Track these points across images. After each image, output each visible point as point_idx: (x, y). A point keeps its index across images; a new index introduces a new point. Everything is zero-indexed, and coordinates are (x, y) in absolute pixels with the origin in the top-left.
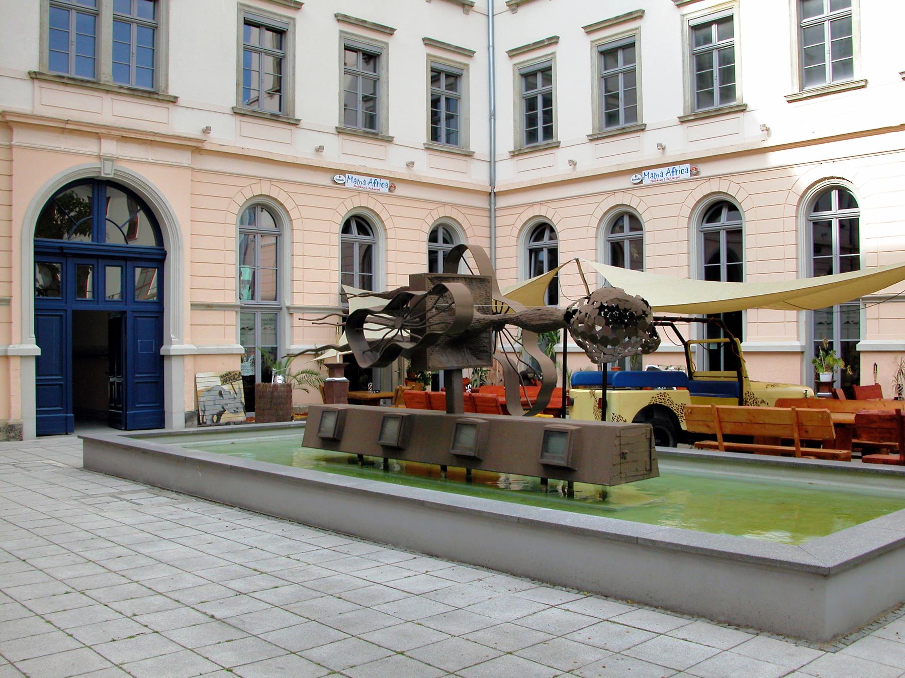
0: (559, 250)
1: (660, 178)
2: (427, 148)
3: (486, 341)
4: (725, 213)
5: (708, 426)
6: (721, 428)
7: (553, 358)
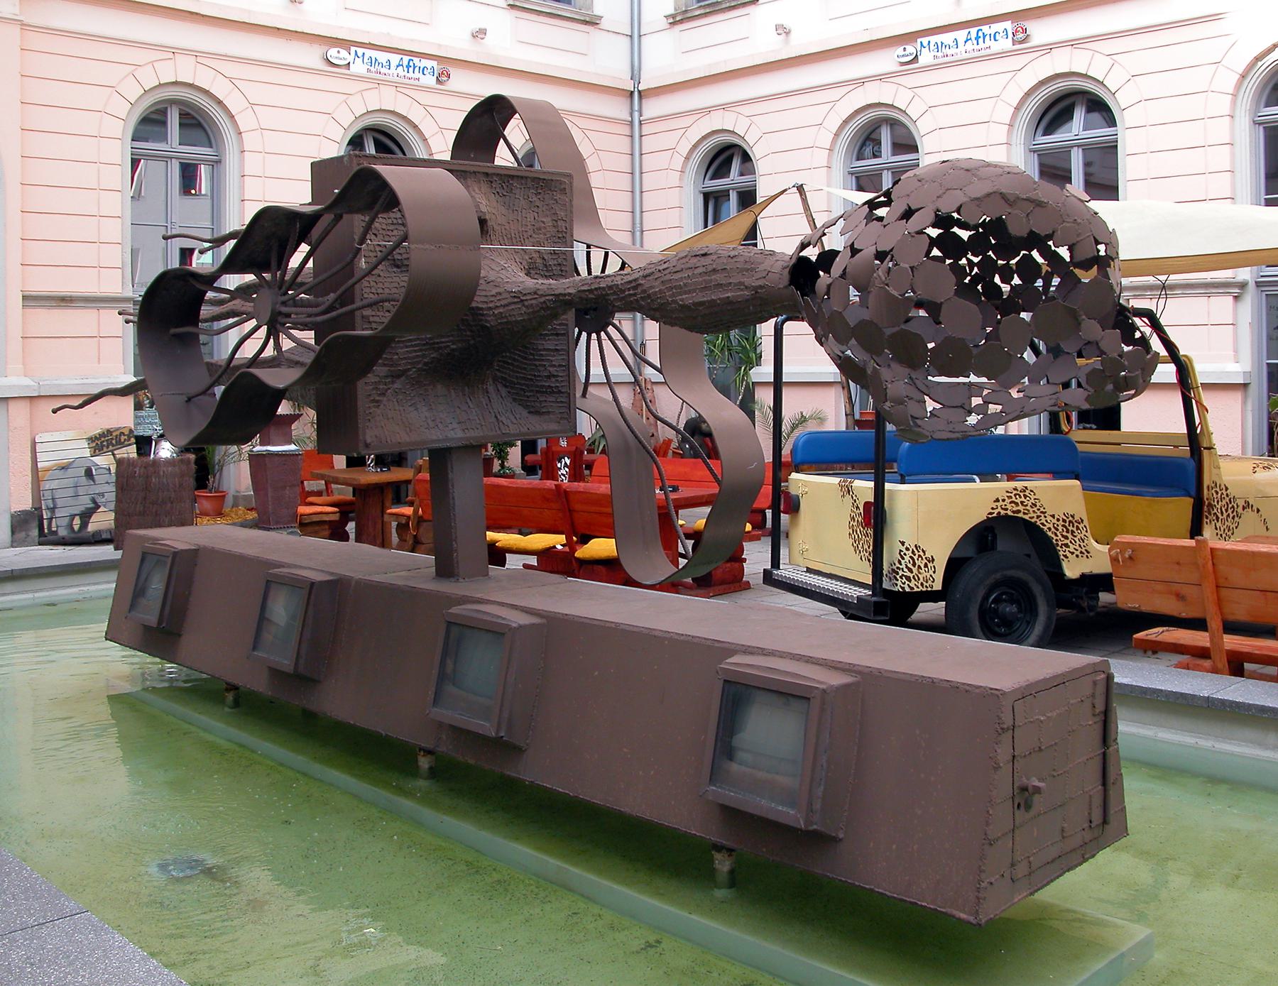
1: (953, 51)
3: (557, 359)
4: (1079, 115)
5: (1180, 597)
6: (1219, 603)
7: (747, 405)
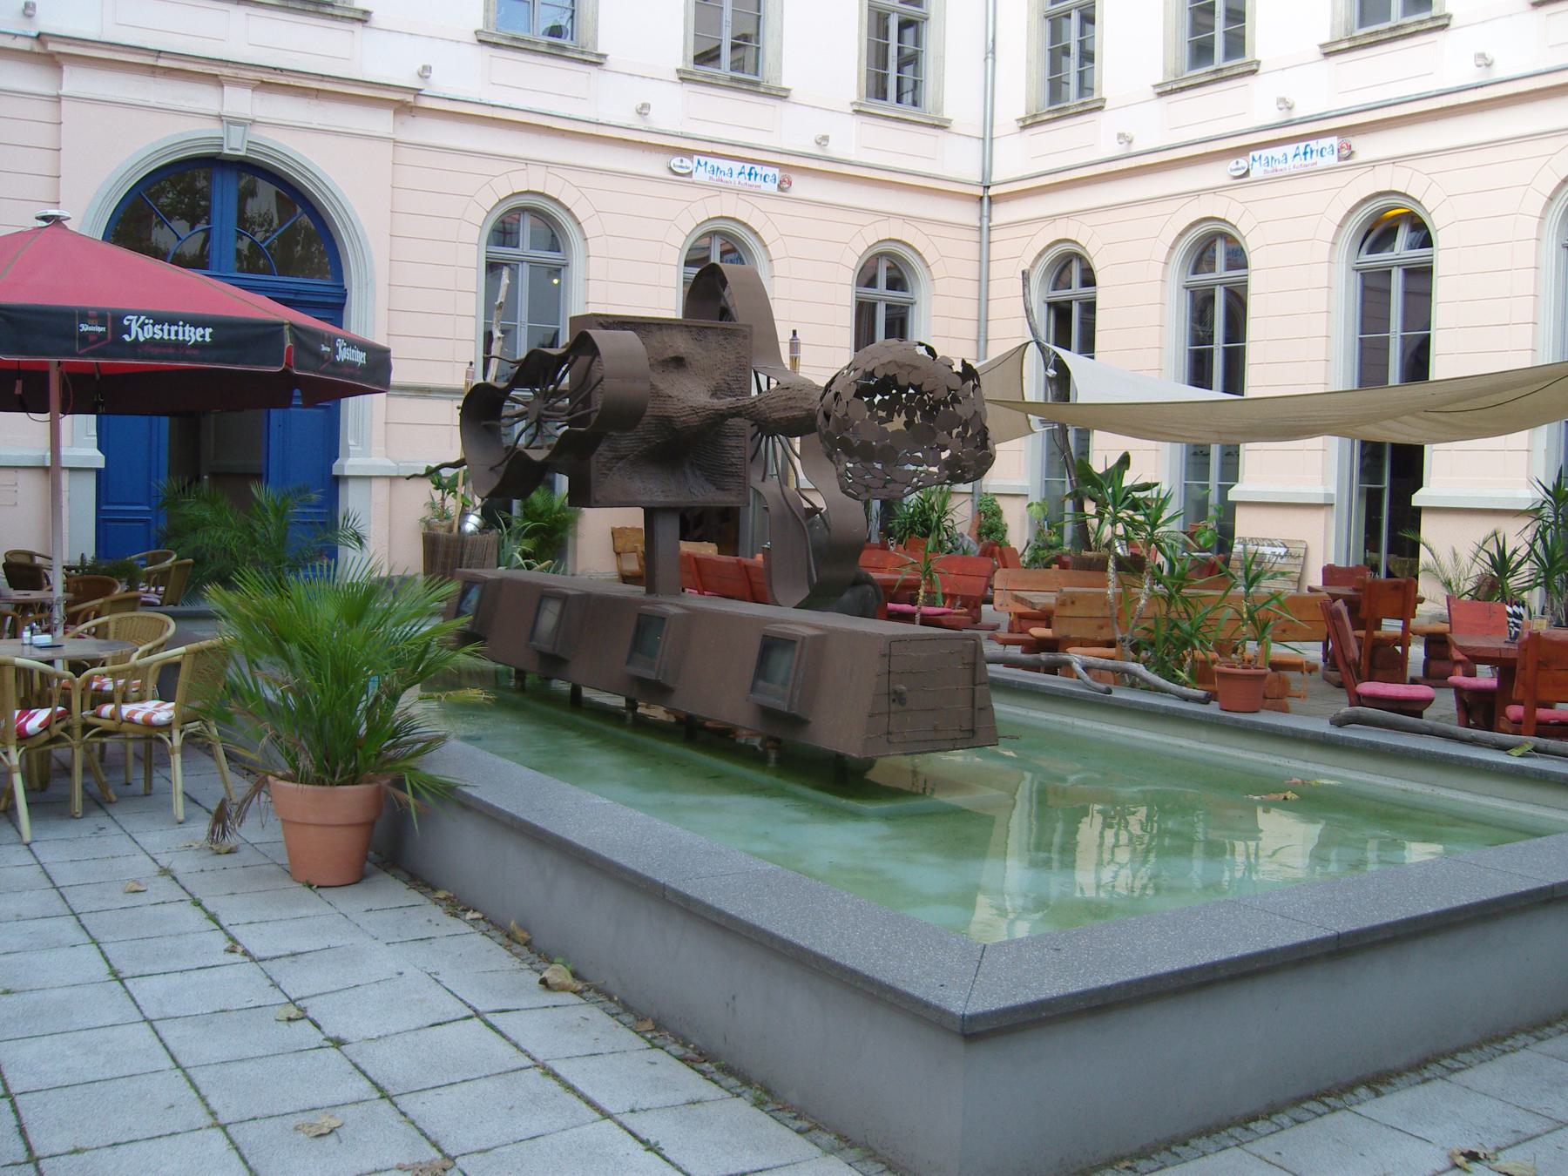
0: (1098, 306)
2: (857, 112)
